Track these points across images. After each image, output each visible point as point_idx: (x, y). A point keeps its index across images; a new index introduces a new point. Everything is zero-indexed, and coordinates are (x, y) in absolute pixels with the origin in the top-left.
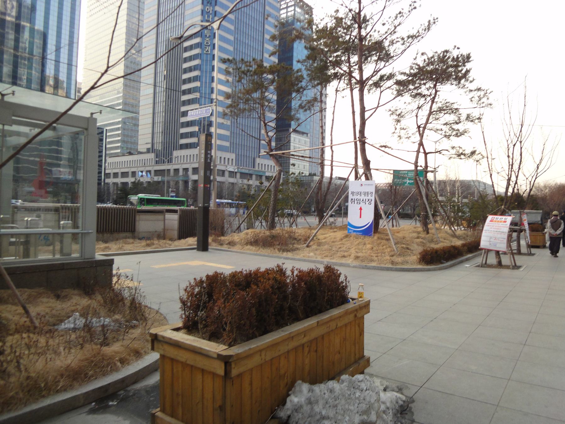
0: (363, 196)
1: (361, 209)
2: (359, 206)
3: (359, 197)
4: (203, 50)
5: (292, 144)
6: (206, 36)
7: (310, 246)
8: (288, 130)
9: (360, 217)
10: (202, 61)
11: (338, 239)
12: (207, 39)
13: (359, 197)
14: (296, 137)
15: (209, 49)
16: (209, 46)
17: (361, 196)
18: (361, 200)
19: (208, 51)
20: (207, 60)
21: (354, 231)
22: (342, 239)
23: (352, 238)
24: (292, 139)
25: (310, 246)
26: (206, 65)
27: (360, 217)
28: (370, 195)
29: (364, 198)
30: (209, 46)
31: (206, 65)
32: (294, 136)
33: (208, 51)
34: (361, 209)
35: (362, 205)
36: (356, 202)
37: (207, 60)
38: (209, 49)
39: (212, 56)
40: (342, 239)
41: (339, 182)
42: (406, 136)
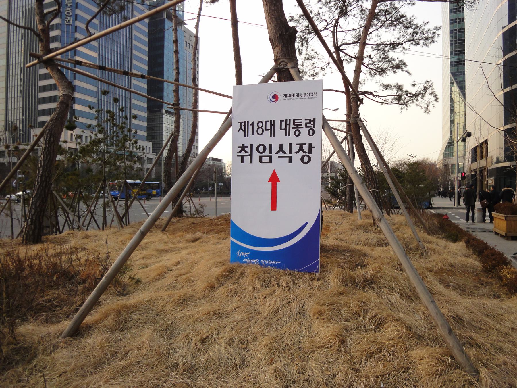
0: (280, 134)
1: (274, 179)
2: (267, 170)
3: (266, 139)
4: (63, 20)
5: (164, 125)
6: (67, 5)
7: (89, 328)
8: (160, 111)
9: (274, 207)
10: (63, 32)
11: (200, 285)
12: (69, 9)
13: (266, 139)
14: (169, 118)
15: (71, 19)
16: (70, 16)
17: (272, 133)
18: (276, 148)
19: (69, 22)
20: (68, 32)
21: (254, 255)
22: (212, 288)
23: (246, 282)
24: (165, 120)
25: (89, 328)
26: (68, 37)
27: (274, 207)
28: (304, 131)
29: (286, 141)
30: (70, 16)
31: (68, 37)
32: (167, 117)
33: (69, 22)
34: (274, 179)
35: (279, 164)
36: (256, 156)
37: (68, 32)
38: (71, 19)
39: (74, 28)
40: (212, 288)
41: (212, 162)
42: (311, 73)
